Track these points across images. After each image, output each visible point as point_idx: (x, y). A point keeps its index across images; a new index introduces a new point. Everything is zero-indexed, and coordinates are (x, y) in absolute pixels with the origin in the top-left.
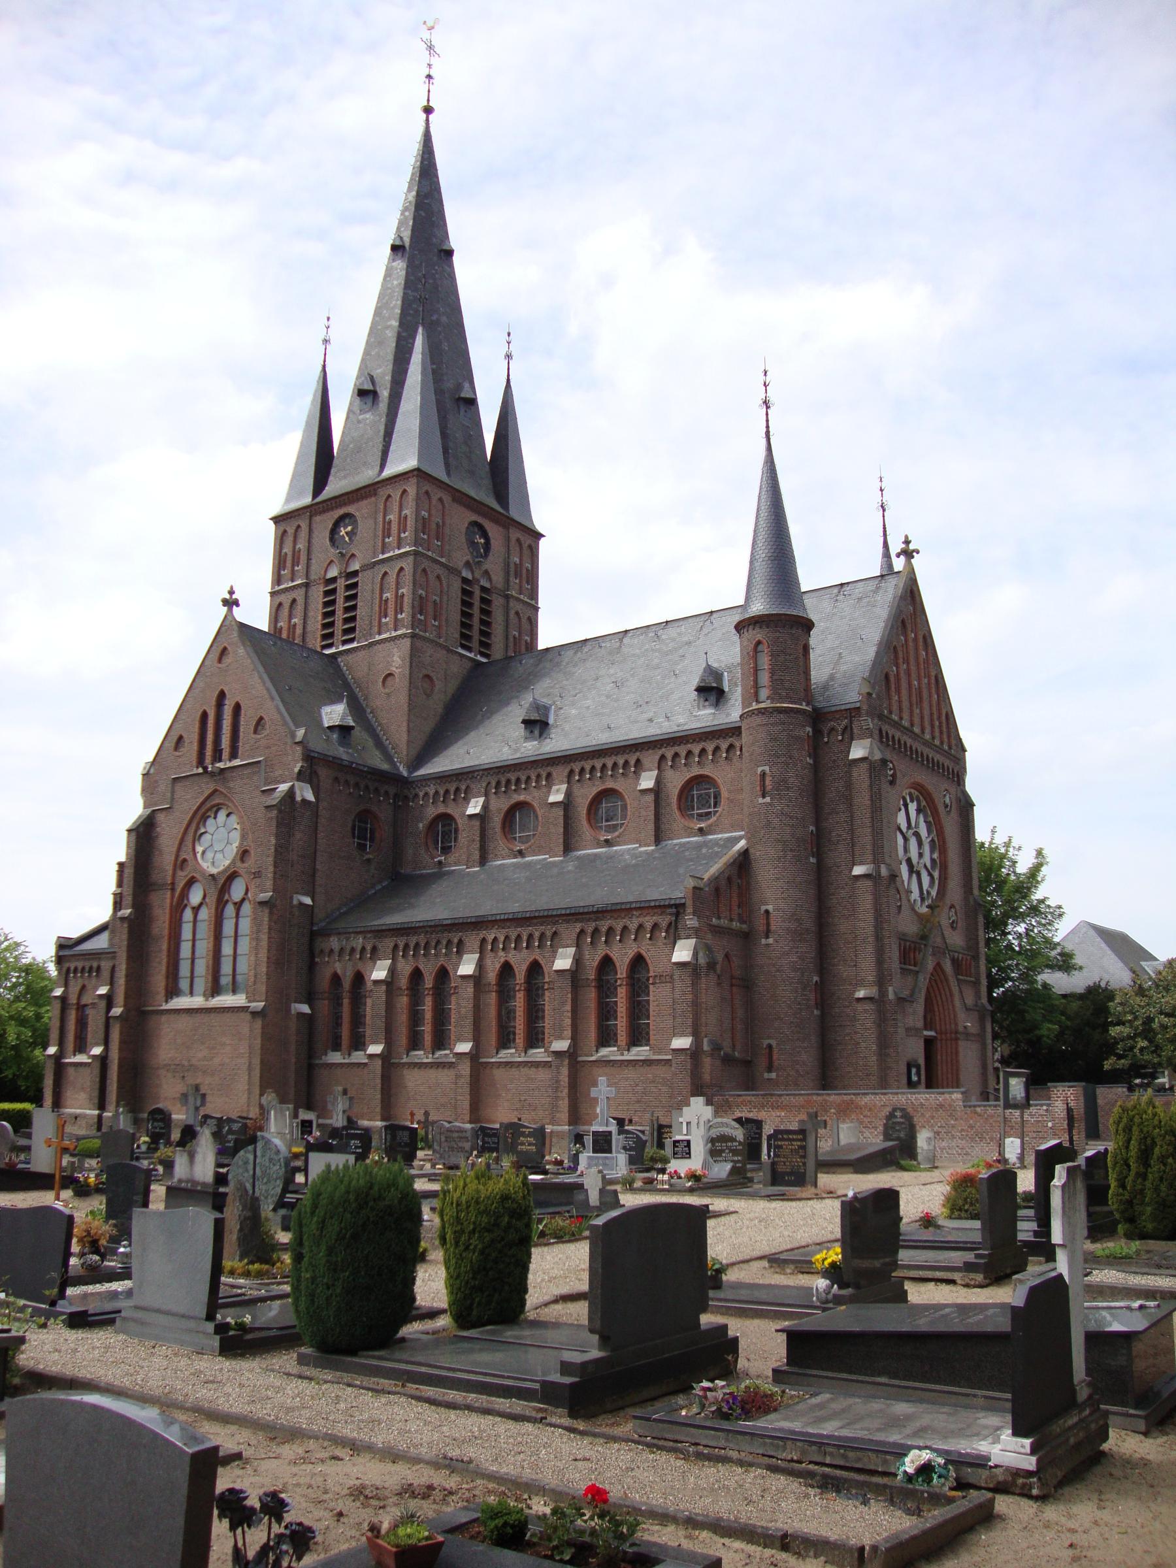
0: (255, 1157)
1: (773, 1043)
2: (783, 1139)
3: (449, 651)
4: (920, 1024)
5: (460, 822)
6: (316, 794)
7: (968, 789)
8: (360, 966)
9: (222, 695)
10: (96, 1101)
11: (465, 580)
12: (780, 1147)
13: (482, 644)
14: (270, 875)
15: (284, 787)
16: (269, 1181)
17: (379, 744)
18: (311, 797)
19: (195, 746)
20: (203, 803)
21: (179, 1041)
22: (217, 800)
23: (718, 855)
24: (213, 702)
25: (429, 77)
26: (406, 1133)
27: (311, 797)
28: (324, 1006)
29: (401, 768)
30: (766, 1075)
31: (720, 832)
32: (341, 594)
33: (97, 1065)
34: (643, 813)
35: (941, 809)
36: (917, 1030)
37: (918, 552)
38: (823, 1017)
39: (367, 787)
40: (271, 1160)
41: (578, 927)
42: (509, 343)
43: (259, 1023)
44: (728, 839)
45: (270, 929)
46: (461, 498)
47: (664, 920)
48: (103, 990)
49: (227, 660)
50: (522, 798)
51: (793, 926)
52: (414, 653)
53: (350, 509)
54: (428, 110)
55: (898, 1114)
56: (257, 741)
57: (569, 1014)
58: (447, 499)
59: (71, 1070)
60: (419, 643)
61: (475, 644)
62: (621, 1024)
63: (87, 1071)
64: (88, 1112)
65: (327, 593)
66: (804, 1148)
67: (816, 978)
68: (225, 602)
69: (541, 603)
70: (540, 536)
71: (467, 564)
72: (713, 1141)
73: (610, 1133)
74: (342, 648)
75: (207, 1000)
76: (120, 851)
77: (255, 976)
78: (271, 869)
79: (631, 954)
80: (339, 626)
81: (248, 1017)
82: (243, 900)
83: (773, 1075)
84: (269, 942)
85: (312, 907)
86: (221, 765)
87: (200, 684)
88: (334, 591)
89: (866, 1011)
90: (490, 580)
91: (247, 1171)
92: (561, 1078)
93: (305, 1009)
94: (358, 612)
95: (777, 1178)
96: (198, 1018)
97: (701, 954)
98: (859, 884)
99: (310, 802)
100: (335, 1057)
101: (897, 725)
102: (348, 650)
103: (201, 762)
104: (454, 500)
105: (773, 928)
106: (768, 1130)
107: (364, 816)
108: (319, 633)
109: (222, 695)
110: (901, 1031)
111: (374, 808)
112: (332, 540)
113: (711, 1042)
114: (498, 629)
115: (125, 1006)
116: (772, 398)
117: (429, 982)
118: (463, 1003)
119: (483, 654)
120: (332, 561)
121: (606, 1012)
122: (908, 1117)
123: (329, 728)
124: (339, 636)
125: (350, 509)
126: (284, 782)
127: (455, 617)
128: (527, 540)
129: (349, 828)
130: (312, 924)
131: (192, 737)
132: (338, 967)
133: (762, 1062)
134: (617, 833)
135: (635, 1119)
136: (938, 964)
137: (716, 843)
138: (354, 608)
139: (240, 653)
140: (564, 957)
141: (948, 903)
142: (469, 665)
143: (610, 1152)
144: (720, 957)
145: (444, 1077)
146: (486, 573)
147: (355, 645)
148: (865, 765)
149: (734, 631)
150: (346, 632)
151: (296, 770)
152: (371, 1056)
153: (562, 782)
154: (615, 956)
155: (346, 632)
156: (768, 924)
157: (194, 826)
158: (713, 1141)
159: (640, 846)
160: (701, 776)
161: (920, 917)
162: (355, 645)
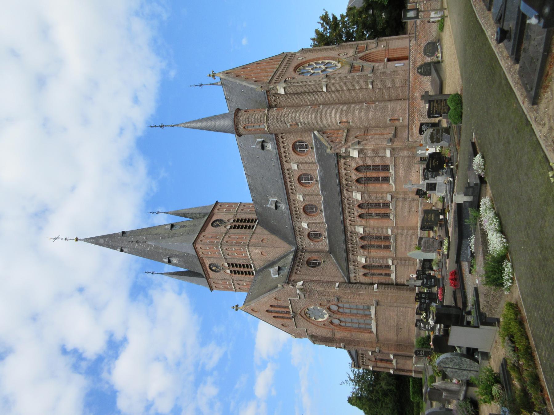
0: (449, 368)
1: (389, 119)
3: (254, 233)
4: (382, 64)
5: (310, 230)
7: (297, 51)
8: (360, 266)
9: (267, 311)
11: (231, 228)
12: (436, 111)
13: (252, 222)
15: (298, 292)
16: (462, 363)
17: (284, 257)
19: (285, 320)
20: (304, 318)
22: (303, 314)
23: (320, 141)
24: (270, 314)
25: (66, 239)
26: (425, 263)
27: (301, 283)
28: (375, 279)
30: (401, 121)
32: (235, 269)
33: (396, 357)
35: (304, 60)
36: (384, 64)
38: (392, 284)
39: (299, 262)
40: (451, 361)
41: (345, 191)
46: (203, 229)
47: (343, 161)
48: (370, 353)
50: (302, 210)
51: (345, 113)
52: (255, 246)
53: (207, 266)
54: (77, 239)
55: (420, 71)
58: (203, 234)
59: (399, 365)
60: (251, 244)
61: (252, 224)
62: (381, 174)
66: (437, 101)
67: (364, 104)
68: (237, 309)
69: (239, 201)
71: (225, 227)
72: (432, 142)
73: (427, 184)
76: (321, 347)
80: (246, 269)
82: (337, 306)
83: (401, 118)
85: (339, 282)
86: (291, 312)
87: (264, 318)
89: (377, 84)
90: (230, 219)
91: (456, 372)
93: (376, 286)
97: (356, 147)
98: (329, 89)
100: (393, 276)
101: (273, 77)
104: (204, 231)
105: (346, 121)
106: (426, 120)
107: (309, 263)
109: (267, 311)
110: (385, 70)
111: (306, 260)
112: (217, 272)
113: (388, 143)
114: (248, 216)
117: (365, 243)
119: (255, 222)
121: (377, 180)
122: (420, 67)
124: (249, 270)
125: (207, 266)
127: (243, 231)
129: (312, 268)
130: (346, 282)
131: (282, 321)
132: (361, 274)
133: (396, 123)
135: (417, 170)
136: (360, 58)
137: (316, 142)
139: (254, 304)
140: (356, 196)
141: (338, 56)
142: (259, 226)
143: (435, 184)
144: (357, 140)
145: (400, 239)
146: (228, 220)
148: (286, 89)
150: (248, 267)
152: (393, 264)
153: (296, 196)
154: (356, 178)
156: (345, 122)
157: (312, 322)
158: (432, 142)
160: (293, 148)
161: (342, 66)
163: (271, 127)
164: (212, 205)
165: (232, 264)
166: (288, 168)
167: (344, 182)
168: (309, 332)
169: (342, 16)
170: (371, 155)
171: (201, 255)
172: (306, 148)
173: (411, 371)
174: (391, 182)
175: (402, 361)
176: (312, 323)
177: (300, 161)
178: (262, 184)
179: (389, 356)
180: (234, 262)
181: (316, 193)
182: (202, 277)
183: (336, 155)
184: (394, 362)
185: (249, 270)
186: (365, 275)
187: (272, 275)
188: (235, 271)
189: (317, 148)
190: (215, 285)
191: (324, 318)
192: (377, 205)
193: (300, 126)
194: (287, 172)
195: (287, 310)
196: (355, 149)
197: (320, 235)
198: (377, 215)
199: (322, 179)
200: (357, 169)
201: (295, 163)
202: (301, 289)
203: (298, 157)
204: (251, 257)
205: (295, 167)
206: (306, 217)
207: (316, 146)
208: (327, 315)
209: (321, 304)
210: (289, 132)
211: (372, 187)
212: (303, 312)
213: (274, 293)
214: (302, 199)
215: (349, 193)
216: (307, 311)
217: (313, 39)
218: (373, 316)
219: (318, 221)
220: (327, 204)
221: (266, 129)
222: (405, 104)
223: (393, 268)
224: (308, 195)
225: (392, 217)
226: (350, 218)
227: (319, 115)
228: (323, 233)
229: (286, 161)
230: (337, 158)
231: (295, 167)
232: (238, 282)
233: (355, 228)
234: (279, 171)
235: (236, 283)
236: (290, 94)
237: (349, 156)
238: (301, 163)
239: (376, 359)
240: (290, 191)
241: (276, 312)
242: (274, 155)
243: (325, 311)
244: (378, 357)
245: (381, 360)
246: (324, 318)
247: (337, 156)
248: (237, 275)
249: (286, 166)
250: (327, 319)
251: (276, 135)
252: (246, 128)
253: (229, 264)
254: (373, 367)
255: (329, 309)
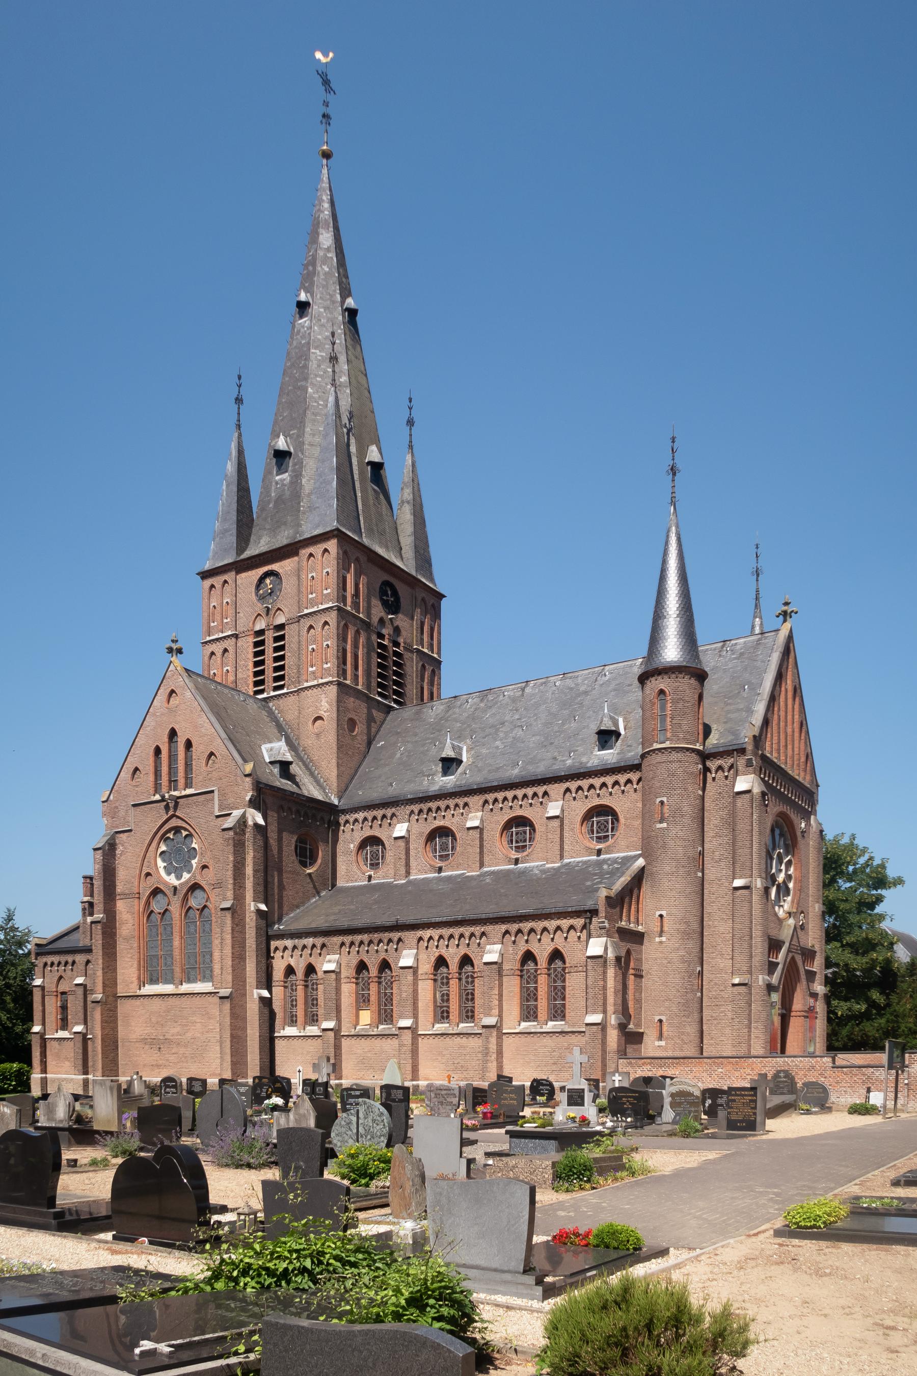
2: (736, 1095)
6: (265, 818)
8: (312, 960)
9: (173, 733)
10: (81, 1068)
14: (231, 887)
15: (237, 813)
18: (261, 821)
19: (151, 778)
21: (154, 1020)
22: (174, 822)
27: (261, 821)
29: (333, 797)
30: (657, 1043)
31: (618, 852)
32: (270, 645)
34: (550, 836)
37: (796, 613)
40: (374, 1121)
41: (504, 927)
42: (410, 408)
43: (227, 1005)
44: (624, 858)
45: (233, 930)
47: (579, 922)
49: (174, 701)
53: (275, 567)
56: (209, 773)
57: (497, 997)
58: (363, 559)
63: (71, 1044)
64: (74, 1077)
65: (256, 644)
69: (447, 658)
70: (441, 596)
73: (583, 1090)
74: (273, 694)
75: (177, 987)
77: (222, 969)
78: (231, 881)
79: (550, 949)
80: (270, 674)
81: (216, 999)
84: (233, 941)
88: (262, 643)
91: (351, 1130)
92: (490, 1046)
93: (265, 993)
94: (266, 666)
95: (732, 1125)
96: (171, 1000)
99: (260, 826)
100: (290, 1031)
102: (279, 695)
103: (157, 788)
105: (666, 929)
108: (252, 679)
109: (173, 733)
115: (103, 993)
116: (679, 466)
118: (404, 988)
120: (259, 615)
121: (528, 997)
123: (271, 763)
124: (270, 683)
126: (237, 808)
128: (431, 600)
132: (443, 951)
134: (525, 853)
137: (615, 861)
138: (282, 658)
147: (285, 691)
149: (636, 682)
150: (276, 679)
151: (248, 798)
152: (324, 1030)
155: (276, 679)
156: (662, 926)
159: (547, 863)
160: (601, 806)
162: (285, 691)
163: (659, 758)
164: (432, 580)
165: (282, 638)
166: (551, 793)
167: (526, 926)
168: (124, 836)
169: (881, 917)
170: (590, 982)
171: (304, 552)
172: (598, 838)
173: (44, 1070)
174: (524, 1025)
175: (72, 1051)
176: (149, 845)
177: (566, 822)
178: (503, 723)
179: (77, 1024)
180: (291, 642)
181: (486, 859)
182: (241, 549)
183: (592, 908)
184: (62, 1034)
185: (270, 683)
186: (290, 971)
187: (268, 746)
188: (262, 643)
189: (600, 864)
190: (218, 586)
191: (169, 874)
192: (469, 996)
193: (659, 826)
194: (540, 790)
195: (181, 782)
196: (606, 949)
197: (375, 865)
198: (446, 998)
199: (523, 872)
200: (556, 955)
201: (563, 811)
202: (242, 821)
203: (579, 819)
204: (306, 688)
205: (554, 809)
206: (421, 834)
207: (605, 861)
208: (176, 883)
209: (205, 867)
210: (646, 799)
211: (512, 986)
212: (180, 823)
213: (221, 746)
214: (469, 824)
215: (500, 935)
216: (184, 833)
217: (883, 866)
218: (186, 988)
219: (413, 863)
220: (461, 883)
221: (656, 746)
222: (691, 1051)
223: (313, 1030)
224: (481, 839)
225: (440, 1027)
226: (436, 938)
227: (682, 870)
228: (381, 873)
229: (568, 790)
230: (586, 911)
231: (554, 809)
232: (231, 650)
233: (410, 948)
234: (541, 769)
235: (229, 644)
236: (734, 803)
237: (589, 936)
238: (562, 826)
239: (63, 993)
240: (490, 797)
241: (172, 758)
242: (584, 760)
243: (186, 876)
244: (70, 998)
245: (64, 1008)
246: (169, 874)
247: (590, 911)
248: (251, 650)
249: (556, 789)
250: (166, 884)
251: (637, 767)
252: (662, 696)
253: (281, 627)
254: (42, 988)
255: (195, 887)
